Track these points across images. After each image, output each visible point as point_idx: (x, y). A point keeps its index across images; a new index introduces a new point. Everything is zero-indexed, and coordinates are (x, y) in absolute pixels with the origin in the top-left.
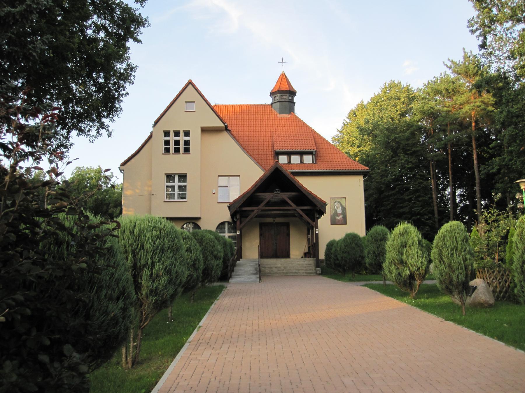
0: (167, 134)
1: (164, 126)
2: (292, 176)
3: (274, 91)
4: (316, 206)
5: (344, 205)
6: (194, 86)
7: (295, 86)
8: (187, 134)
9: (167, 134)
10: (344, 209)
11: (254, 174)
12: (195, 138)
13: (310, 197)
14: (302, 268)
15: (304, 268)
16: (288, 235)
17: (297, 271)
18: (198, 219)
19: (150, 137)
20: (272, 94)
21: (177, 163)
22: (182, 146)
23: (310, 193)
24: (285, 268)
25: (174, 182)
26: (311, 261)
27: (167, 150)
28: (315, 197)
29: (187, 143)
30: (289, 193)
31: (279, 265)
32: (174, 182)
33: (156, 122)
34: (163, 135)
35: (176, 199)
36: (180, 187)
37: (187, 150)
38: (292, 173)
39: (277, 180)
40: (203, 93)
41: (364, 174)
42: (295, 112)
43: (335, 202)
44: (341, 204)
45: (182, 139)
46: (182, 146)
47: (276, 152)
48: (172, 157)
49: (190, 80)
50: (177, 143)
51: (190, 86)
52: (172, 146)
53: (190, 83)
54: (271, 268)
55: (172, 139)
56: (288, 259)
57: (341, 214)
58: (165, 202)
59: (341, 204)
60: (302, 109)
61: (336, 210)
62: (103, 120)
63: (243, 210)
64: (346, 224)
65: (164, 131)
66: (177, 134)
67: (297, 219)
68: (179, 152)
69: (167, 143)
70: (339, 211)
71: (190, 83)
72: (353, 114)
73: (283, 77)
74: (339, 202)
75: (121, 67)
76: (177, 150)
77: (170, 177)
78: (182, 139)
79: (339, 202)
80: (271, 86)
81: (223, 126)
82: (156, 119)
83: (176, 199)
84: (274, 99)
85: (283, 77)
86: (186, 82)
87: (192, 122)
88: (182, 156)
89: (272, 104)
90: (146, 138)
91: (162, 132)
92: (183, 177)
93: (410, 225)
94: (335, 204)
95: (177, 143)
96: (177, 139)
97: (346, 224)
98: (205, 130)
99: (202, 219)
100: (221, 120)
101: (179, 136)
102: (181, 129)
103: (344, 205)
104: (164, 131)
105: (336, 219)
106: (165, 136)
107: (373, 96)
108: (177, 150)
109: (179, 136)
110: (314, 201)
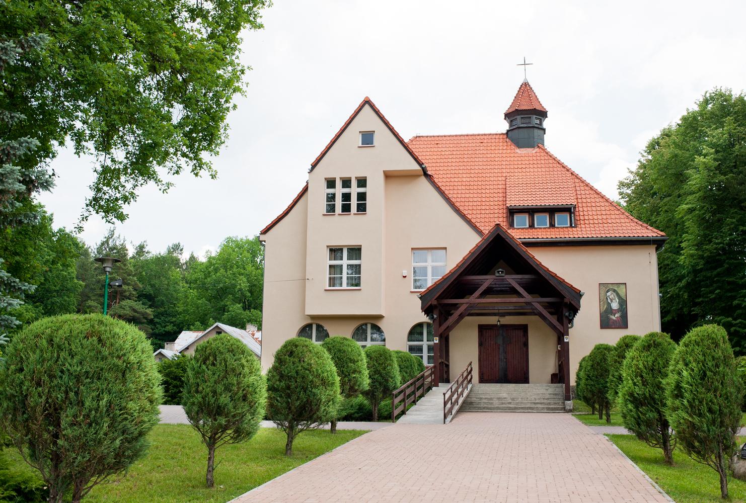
0: (331, 183)
1: (327, 169)
2: (524, 248)
3: (510, 111)
4: (562, 297)
5: (623, 295)
6: (373, 107)
7: (546, 102)
8: (362, 182)
9: (331, 183)
10: (623, 303)
11: (463, 244)
12: (375, 190)
13: (553, 282)
14: (543, 401)
15: (545, 401)
16: (526, 344)
17: (533, 406)
18: (380, 317)
19: (305, 190)
20: (508, 116)
21: (346, 229)
22: (354, 202)
23: (554, 276)
24: (513, 399)
25: (342, 259)
26: (559, 388)
27: (331, 209)
28: (562, 282)
29: (362, 197)
30: (520, 276)
31: (505, 395)
32: (342, 259)
33: (314, 166)
34: (325, 184)
35: (345, 286)
36: (350, 267)
37: (362, 208)
38: (524, 244)
39: (497, 253)
40: (387, 117)
41: (658, 243)
42: (545, 144)
43: (608, 291)
44: (618, 295)
45: (354, 190)
46: (354, 202)
47: (510, 209)
48: (339, 220)
49: (367, 97)
50: (346, 197)
51: (367, 106)
52: (339, 203)
53: (367, 102)
54: (491, 399)
55: (339, 191)
56: (526, 385)
57: (618, 311)
58: (411, 292)
59: (618, 295)
60: (557, 137)
61: (609, 304)
62: (83, 143)
63: (444, 302)
64: (602, 327)
65: (326, 179)
66: (346, 183)
67: (537, 317)
68: (350, 211)
69: (331, 198)
70: (615, 305)
71: (367, 102)
72: (653, 146)
73: (525, 89)
74: (614, 291)
75: (224, 73)
76: (346, 208)
77: (335, 252)
78: (354, 190)
79: (614, 291)
80: (506, 104)
81: (417, 167)
82: (313, 160)
83: (345, 286)
84: (511, 126)
85: (525, 89)
86: (361, 100)
87: (371, 164)
88: (353, 218)
89: (508, 131)
90: (300, 190)
91: (324, 179)
92: (355, 252)
93: (142, 333)
94: (608, 294)
95: (346, 197)
96: (346, 190)
97: (602, 327)
98: (389, 176)
99: (384, 319)
100: (416, 159)
101: (350, 187)
102: (353, 175)
103: (618, 293)
104: (326, 179)
105: (608, 318)
106: (328, 187)
107: (686, 114)
108: (346, 208)
109: (350, 187)
110: (559, 288)
